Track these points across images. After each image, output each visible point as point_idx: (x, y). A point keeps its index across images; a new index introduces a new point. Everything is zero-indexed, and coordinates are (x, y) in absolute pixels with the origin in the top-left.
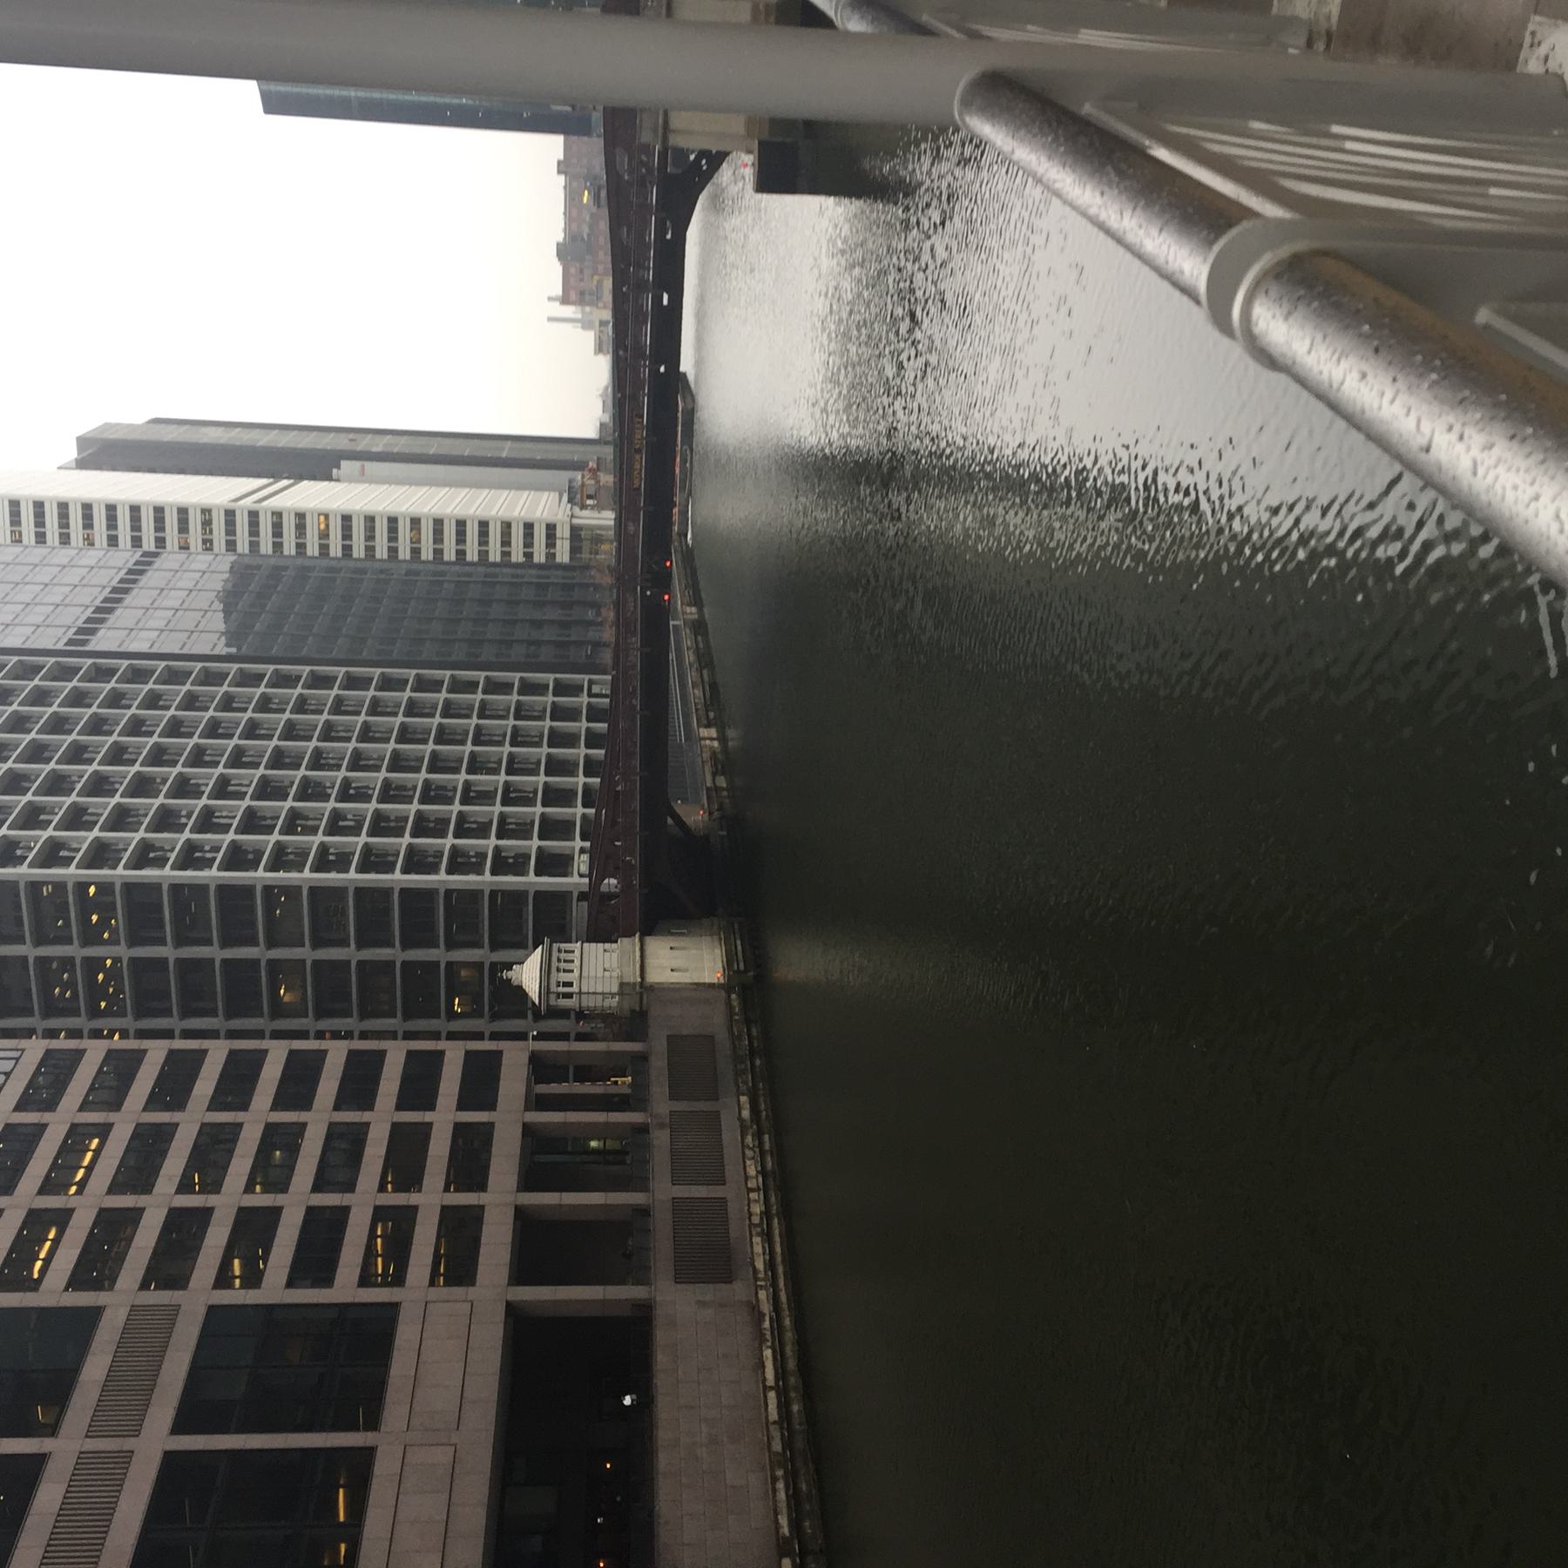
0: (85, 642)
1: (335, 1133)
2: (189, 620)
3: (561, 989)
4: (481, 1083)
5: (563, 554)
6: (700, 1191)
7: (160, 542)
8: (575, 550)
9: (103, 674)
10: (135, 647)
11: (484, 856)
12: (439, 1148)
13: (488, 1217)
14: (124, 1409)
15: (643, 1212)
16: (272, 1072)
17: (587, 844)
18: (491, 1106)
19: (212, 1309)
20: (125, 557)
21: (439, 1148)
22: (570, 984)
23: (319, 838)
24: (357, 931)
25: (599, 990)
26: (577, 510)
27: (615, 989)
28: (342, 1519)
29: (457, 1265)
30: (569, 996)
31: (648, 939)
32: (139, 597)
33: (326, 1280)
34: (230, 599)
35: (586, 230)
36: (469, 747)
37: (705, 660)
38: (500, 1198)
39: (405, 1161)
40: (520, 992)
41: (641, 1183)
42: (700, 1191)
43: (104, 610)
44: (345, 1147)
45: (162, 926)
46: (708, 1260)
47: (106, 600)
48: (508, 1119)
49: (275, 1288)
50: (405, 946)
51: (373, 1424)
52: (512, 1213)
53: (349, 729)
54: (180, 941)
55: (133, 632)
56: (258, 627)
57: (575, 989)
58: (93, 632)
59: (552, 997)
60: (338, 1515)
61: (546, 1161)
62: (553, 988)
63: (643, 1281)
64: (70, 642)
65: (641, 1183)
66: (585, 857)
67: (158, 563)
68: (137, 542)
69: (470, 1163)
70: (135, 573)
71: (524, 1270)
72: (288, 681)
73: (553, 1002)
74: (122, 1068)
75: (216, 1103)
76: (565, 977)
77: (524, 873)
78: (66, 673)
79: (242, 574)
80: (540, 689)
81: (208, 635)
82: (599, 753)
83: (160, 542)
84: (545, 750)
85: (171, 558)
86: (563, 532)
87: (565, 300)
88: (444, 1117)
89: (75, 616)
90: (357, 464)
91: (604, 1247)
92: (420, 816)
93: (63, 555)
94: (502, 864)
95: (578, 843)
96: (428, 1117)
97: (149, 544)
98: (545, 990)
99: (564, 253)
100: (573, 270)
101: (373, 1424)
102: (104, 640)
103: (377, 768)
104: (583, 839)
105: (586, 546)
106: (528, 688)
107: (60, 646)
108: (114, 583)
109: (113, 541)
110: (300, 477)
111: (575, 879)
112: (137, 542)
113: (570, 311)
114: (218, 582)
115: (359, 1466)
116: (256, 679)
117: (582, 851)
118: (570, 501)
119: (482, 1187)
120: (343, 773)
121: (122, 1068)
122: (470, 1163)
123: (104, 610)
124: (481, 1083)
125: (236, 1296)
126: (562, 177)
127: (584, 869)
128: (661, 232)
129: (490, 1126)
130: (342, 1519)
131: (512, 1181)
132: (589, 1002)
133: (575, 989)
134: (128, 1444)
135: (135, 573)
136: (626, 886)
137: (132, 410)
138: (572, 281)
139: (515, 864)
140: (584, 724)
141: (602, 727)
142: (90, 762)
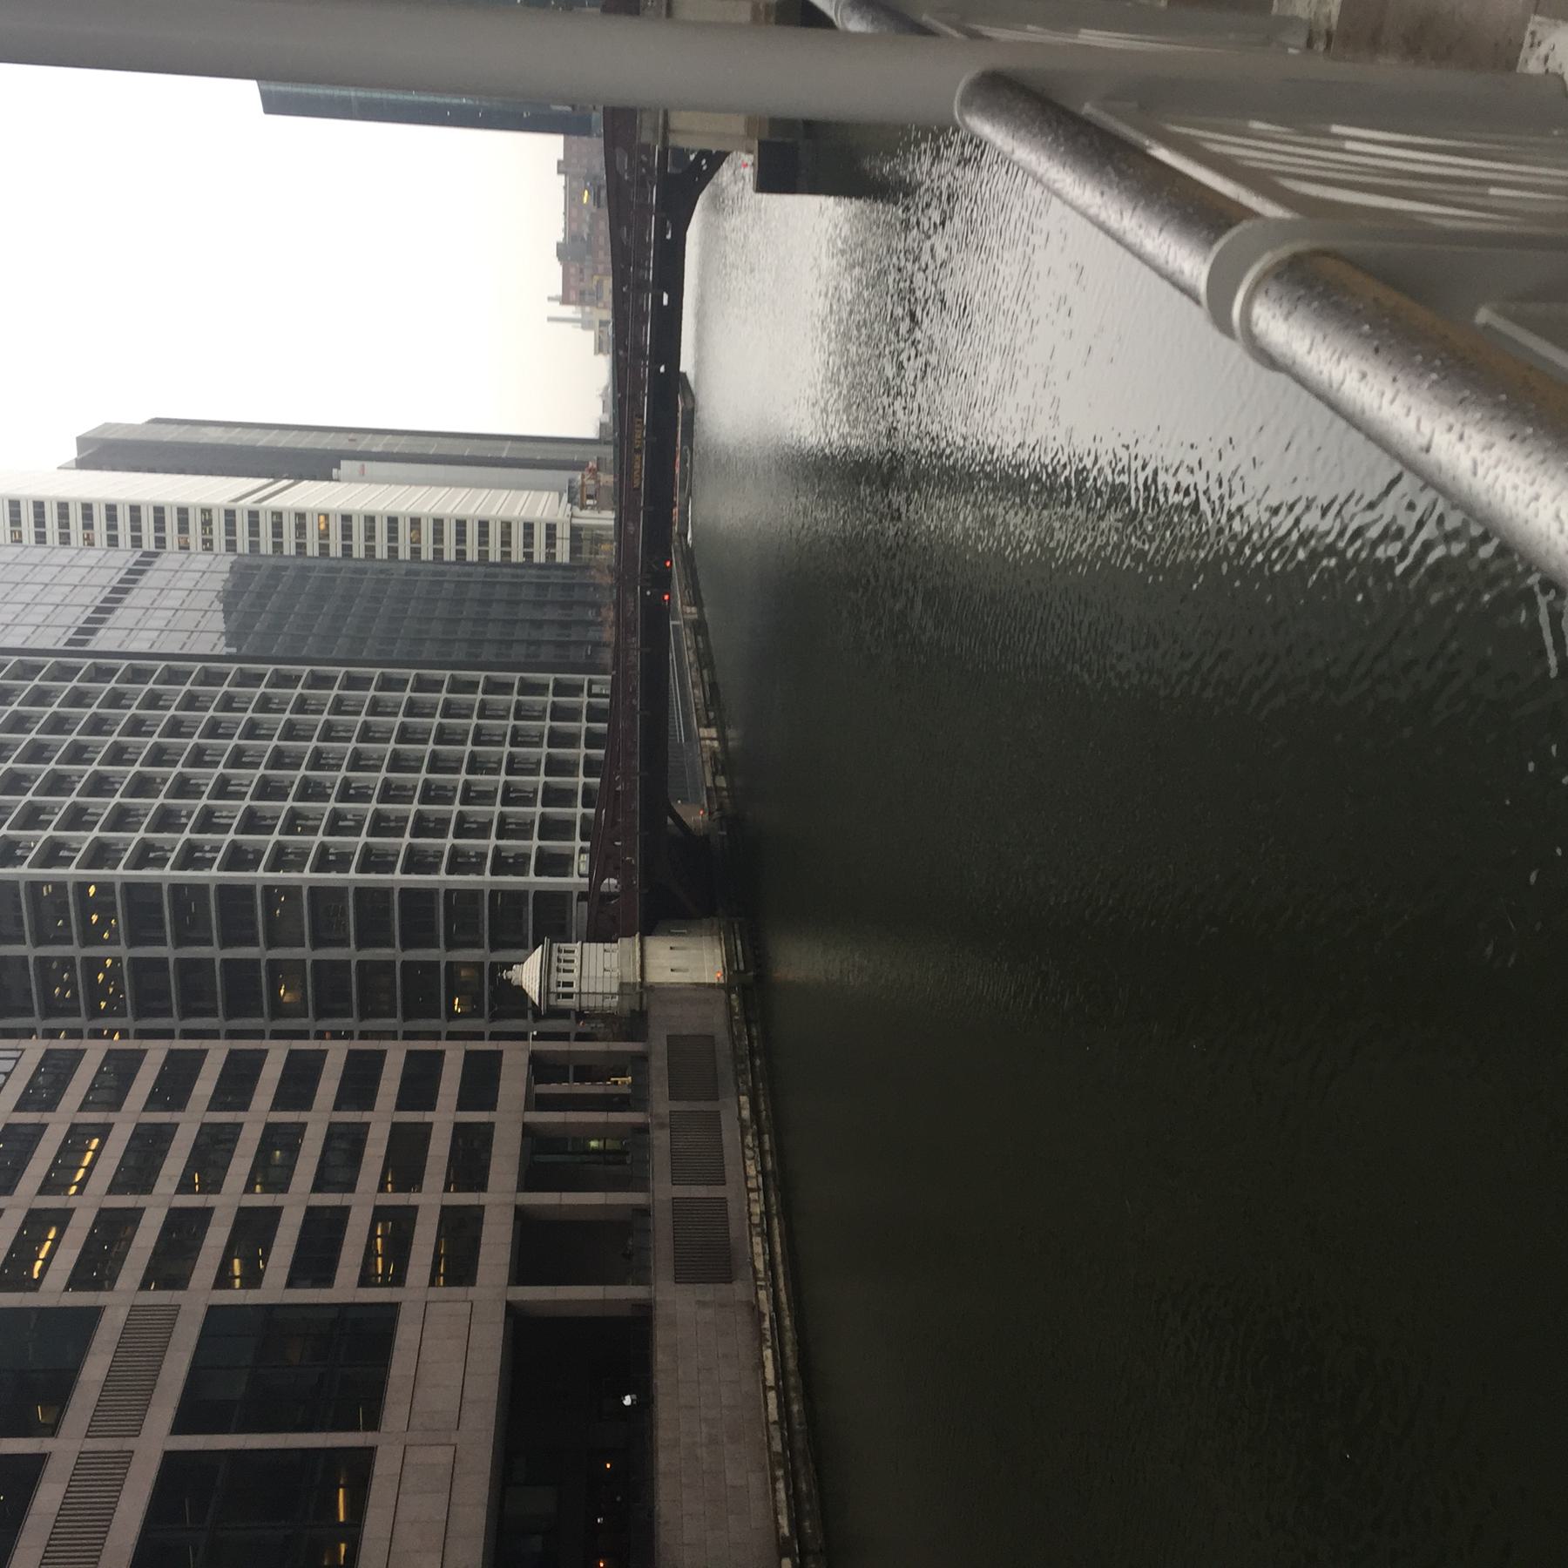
0: (85, 642)
1: (335, 1133)
2: (189, 620)
3: (561, 989)
4: (481, 1083)
5: (563, 554)
6: (700, 1191)
7: (160, 542)
8: (575, 550)
9: (103, 674)
10: (135, 647)
11: (484, 856)
12: (439, 1148)
13: (488, 1217)
14: (124, 1409)
15: (643, 1212)
16: (272, 1072)
17: (587, 844)
18: (491, 1106)
19: (212, 1309)
20: (125, 557)
21: (439, 1148)
22: (570, 984)
24: (357, 931)
25: (599, 990)
26: (577, 510)
27: (615, 989)
28: (342, 1519)
29: (457, 1265)
30: (569, 996)
31: (648, 939)
32: (139, 597)
33: (326, 1280)
35: (586, 230)
37: (705, 660)
38: (500, 1198)
39: (405, 1161)
40: (520, 992)
41: (641, 1183)
42: (700, 1191)
43: (104, 610)
44: (345, 1147)
45: (162, 926)
46: (708, 1260)
47: (106, 600)
48: (508, 1119)
49: (275, 1288)
51: (373, 1424)
53: (349, 729)
54: (180, 941)
55: (133, 632)
56: (258, 627)
57: (575, 989)
58: (93, 632)
59: (552, 997)
60: (338, 1515)
61: (546, 1161)
62: (553, 988)
63: (643, 1281)
64: (70, 642)
65: (641, 1183)
66: (585, 857)
67: (158, 563)
68: (137, 542)
69: (470, 1163)
70: (135, 573)
71: (524, 1270)
72: (288, 681)
73: (553, 1002)
74: (122, 1068)
75: (216, 1103)
76: (565, 977)
77: (524, 873)
78: (66, 673)
79: (242, 574)
80: (540, 689)
81: (208, 635)
82: (599, 753)
83: (160, 542)
85: (171, 558)
86: (563, 532)
87: (565, 300)
89: (75, 616)
90: (357, 464)
91: (604, 1247)
93: (63, 555)
94: (502, 864)
95: (578, 843)
96: (428, 1117)
97: (149, 544)
98: (545, 990)
99: (564, 253)
100: (573, 270)
101: (373, 1424)
102: (104, 640)
103: (377, 768)
104: (583, 839)
105: (586, 546)
106: (528, 688)
107: (60, 646)
108: (114, 583)
109: (113, 541)
110: (300, 477)
111: (575, 879)
112: (137, 542)
113: (570, 311)
114: (218, 582)
115: (359, 1466)
116: (256, 679)
117: (582, 851)
118: (570, 501)
119: (482, 1187)
120: (343, 773)
121: (122, 1068)
122: (470, 1163)
123: (104, 610)
124: (481, 1083)
125: (236, 1296)
126: (562, 177)
127: (584, 869)
129: (490, 1126)
130: (342, 1519)
131: (512, 1181)
132: (589, 1002)
133: (575, 989)
134: (128, 1444)
135: (135, 573)
137: (132, 410)
138: (572, 281)
139: (515, 864)
140: (584, 724)
141: (602, 727)
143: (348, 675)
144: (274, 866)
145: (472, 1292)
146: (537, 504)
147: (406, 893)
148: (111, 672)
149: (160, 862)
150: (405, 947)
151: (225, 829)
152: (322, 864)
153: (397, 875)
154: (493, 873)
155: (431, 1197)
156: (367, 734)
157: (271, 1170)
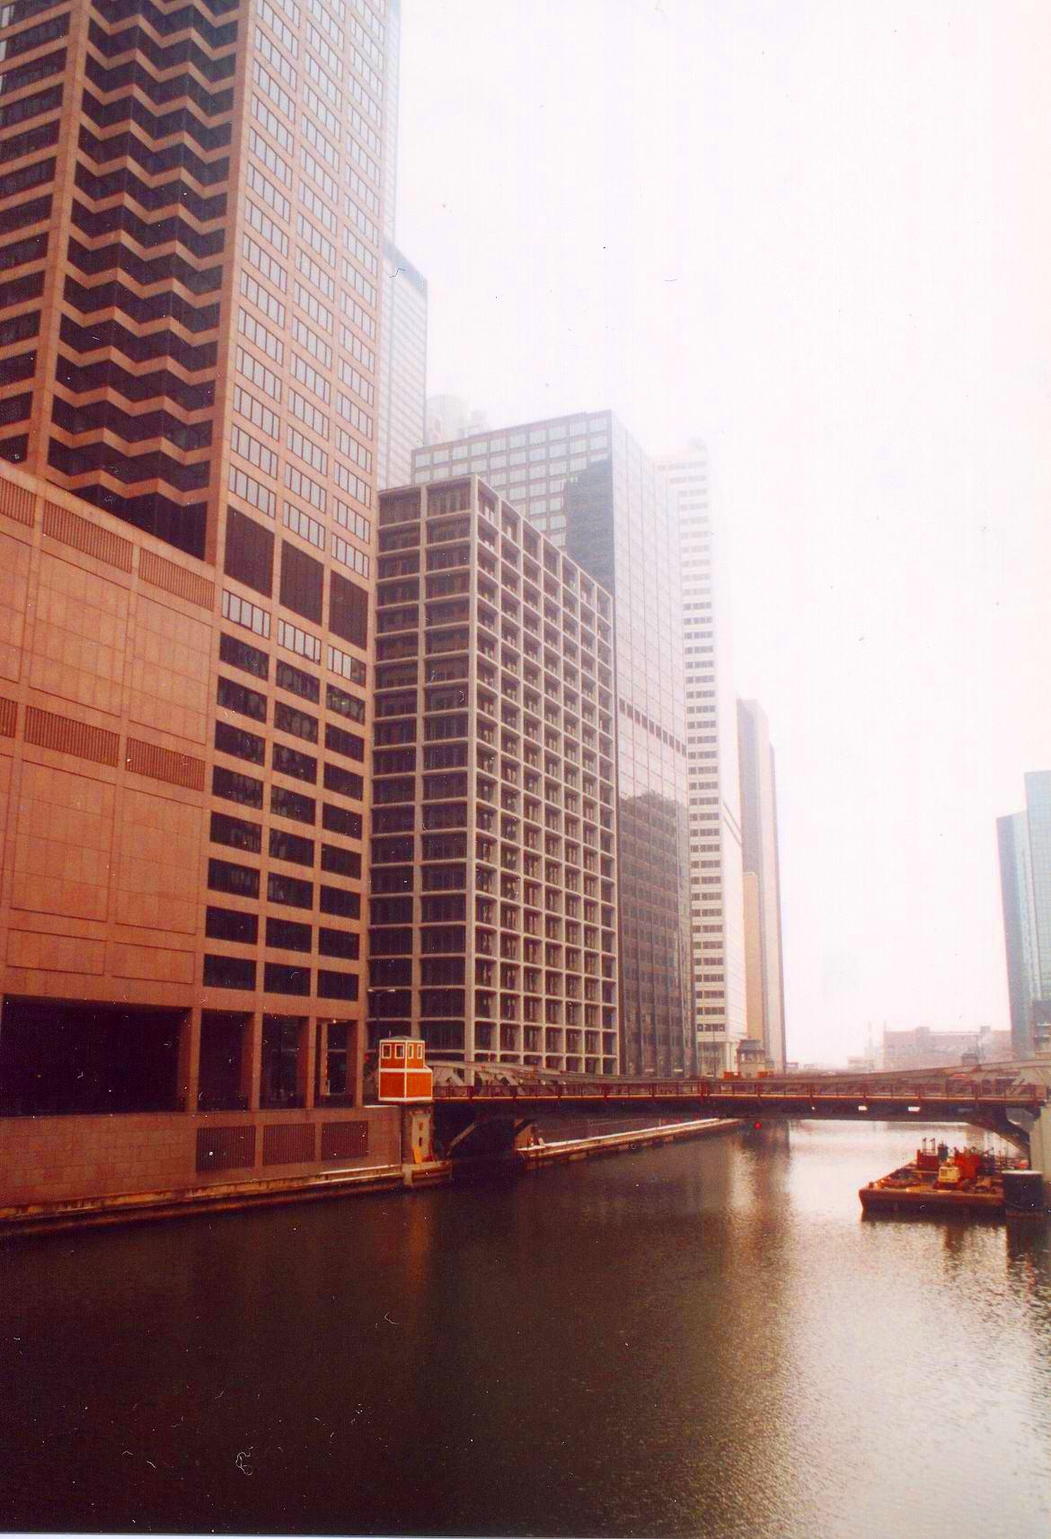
1: (305, 930)
2: (641, 776)
4: (338, 986)
5: (702, 1037)
6: (259, 1147)
7: (692, 756)
8: (705, 1046)
9: (606, 723)
10: (621, 742)
11: (489, 984)
12: (294, 958)
13: (247, 993)
15: (244, 1105)
20: (681, 734)
21: (294, 958)
23: (522, 876)
24: (435, 897)
26: (735, 1047)
32: (655, 742)
34: (650, 798)
36: (584, 975)
37: (636, 1147)
38: (261, 1002)
39: (288, 935)
41: (265, 1103)
42: (259, 1147)
43: (644, 721)
44: (297, 893)
45: (437, 767)
46: (216, 1153)
48: (314, 1006)
50: (423, 929)
52: (184, 1004)
53: (575, 887)
54: (426, 779)
55: (630, 741)
56: (638, 822)
58: (630, 715)
61: (283, 1031)
63: (202, 1107)
64: (622, 702)
65: (265, 1103)
67: (679, 755)
68: (691, 740)
69: (286, 980)
70: (672, 742)
71: (210, 1017)
72: (606, 844)
74: (351, 746)
75: (328, 809)
77: (478, 1013)
78: (604, 699)
79: (670, 809)
80: (608, 1023)
81: (628, 788)
83: (692, 756)
84: (522, 1023)
85: (683, 763)
86: (719, 1037)
88: (262, 953)
89: (640, 705)
91: (224, 1090)
92: (491, 933)
93: (680, 695)
94: (483, 997)
96: (315, 949)
97: (691, 748)
99: (921, 1033)
102: (625, 723)
103: (548, 907)
105: (711, 1054)
106: (608, 1013)
107: (620, 696)
109: (691, 725)
110: (743, 846)
112: (691, 740)
114: (668, 793)
116: (606, 822)
118: (743, 1042)
120: (544, 883)
121: (351, 746)
122: (286, 980)
123: (644, 721)
124: (338, 986)
128: (964, 1104)
129: (307, 993)
131: (272, 960)
134: (123, 741)
135: (672, 742)
136: (582, 1076)
137: (776, 732)
139: (483, 1009)
140: (584, 1056)
142: (526, 706)
143: (611, 860)
144: (480, 931)
145: (211, 745)
146: (737, 1024)
147: (461, 1026)
148: (607, 800)
149: (481, 794)
150: (423, 899)
151: (505, 776)
152: (481, 933)
153: (475, 955)
154: (477, 1024)
155: (265, 863)
156: (572, 926)
157: (286, 718)
